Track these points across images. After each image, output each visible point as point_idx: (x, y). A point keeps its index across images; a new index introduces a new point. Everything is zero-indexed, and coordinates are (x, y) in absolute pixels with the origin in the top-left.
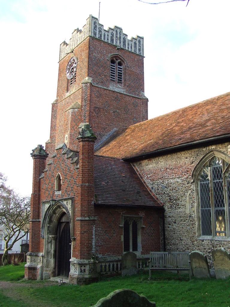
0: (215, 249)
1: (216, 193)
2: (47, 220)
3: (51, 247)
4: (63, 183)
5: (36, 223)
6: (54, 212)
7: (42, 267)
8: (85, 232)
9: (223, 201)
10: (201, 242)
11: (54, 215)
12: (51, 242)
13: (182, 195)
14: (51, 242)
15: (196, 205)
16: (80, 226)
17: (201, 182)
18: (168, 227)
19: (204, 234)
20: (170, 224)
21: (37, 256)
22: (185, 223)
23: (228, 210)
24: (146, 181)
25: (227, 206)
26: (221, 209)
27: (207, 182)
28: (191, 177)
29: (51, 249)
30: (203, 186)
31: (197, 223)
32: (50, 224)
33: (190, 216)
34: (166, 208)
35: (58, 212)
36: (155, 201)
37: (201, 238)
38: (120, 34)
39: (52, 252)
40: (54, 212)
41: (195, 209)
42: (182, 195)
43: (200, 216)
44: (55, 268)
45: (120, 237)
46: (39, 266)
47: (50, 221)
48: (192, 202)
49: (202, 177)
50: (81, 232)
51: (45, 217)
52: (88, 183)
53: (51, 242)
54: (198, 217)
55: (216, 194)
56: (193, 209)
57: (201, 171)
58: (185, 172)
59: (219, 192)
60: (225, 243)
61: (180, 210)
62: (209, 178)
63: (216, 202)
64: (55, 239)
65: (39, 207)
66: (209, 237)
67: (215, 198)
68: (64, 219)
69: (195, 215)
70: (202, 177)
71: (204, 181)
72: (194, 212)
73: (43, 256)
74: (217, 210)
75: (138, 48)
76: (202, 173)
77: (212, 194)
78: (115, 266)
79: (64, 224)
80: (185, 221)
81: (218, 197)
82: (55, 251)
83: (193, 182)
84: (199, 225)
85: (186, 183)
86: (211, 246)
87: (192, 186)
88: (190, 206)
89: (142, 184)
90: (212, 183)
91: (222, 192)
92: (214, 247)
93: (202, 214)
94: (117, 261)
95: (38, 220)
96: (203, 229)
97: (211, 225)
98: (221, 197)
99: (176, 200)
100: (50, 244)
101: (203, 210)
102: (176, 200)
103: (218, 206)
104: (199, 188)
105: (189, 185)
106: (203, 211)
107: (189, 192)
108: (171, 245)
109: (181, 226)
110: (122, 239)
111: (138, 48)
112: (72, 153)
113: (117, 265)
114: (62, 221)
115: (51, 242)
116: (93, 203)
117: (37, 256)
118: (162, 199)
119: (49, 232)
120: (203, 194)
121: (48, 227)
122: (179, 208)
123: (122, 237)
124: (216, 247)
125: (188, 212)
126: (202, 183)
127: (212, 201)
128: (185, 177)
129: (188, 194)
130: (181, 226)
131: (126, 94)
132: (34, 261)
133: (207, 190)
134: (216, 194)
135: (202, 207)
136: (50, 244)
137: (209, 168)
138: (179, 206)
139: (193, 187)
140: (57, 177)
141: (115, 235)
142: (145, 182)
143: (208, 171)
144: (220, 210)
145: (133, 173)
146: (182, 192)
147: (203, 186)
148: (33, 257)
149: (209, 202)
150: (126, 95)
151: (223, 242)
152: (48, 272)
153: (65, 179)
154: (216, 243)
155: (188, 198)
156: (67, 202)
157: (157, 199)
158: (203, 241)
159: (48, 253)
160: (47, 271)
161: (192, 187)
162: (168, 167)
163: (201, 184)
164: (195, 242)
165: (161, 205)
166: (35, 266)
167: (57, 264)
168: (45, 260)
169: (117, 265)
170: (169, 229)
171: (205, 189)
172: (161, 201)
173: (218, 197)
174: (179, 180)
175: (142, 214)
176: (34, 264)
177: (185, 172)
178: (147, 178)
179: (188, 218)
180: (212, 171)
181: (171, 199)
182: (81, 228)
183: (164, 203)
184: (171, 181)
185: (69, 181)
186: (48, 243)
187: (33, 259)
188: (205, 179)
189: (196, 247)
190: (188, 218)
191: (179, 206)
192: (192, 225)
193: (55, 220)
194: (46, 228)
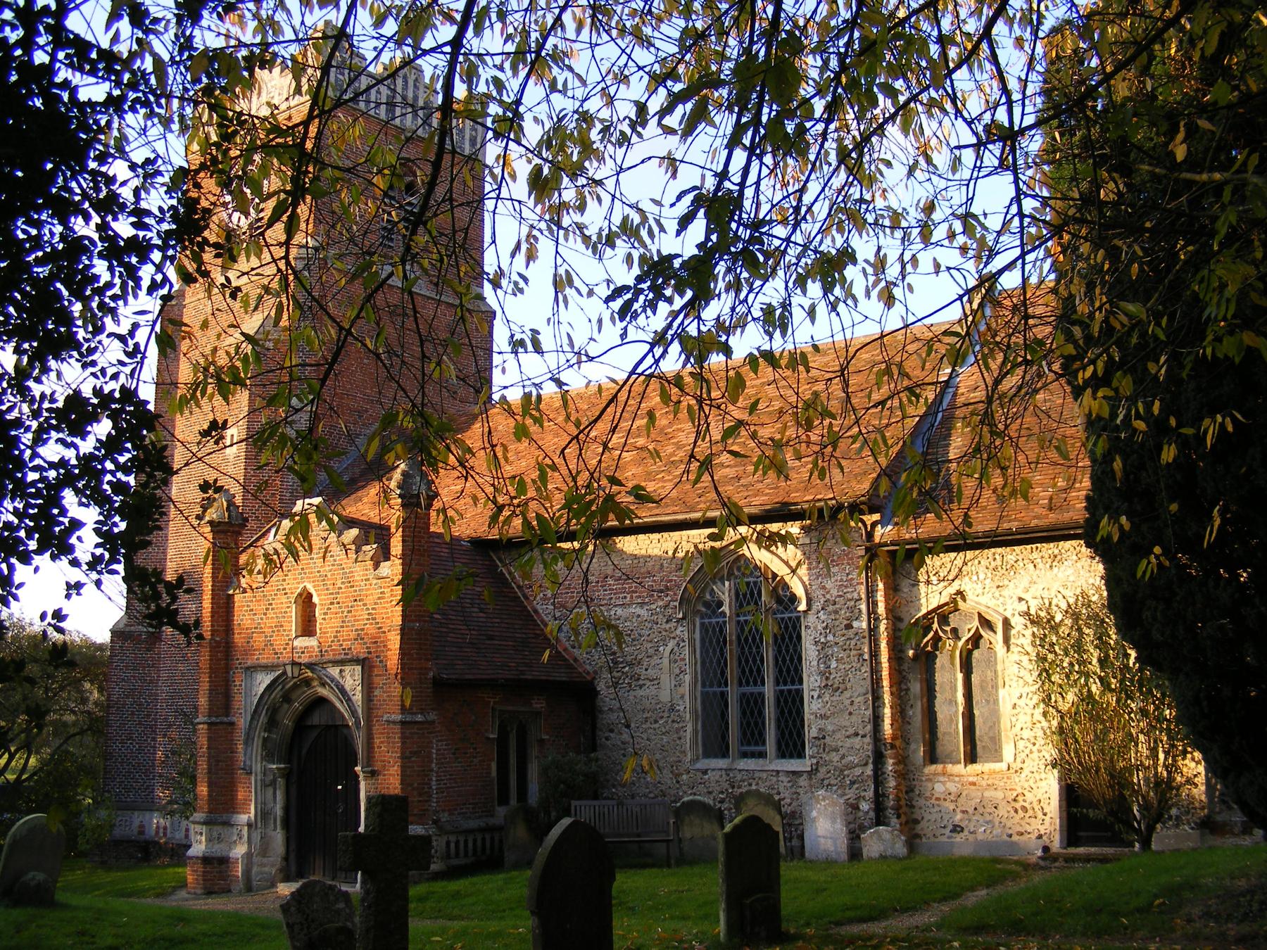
0: (737, 791)
1: (743, 648)
2: (263, 718)
3: (275, 797)
4: (325, 614)
5: (221, 727)
6: (287, 698)
7: (248, 855)
8: (413, 753)
9: (759, 671)
10: (699, 774)
11: (286, 706)
12: (273, 783)
13: (651, 651)
14: (273, 783)
15: (687, 678)
16: (402, 738)
17: (702, 618)
18: (607, 739)
19: (707, 754)
20: (612, 731)
21: (228, 824)
22: (657, 726)
23: (772, 693)
24: (538, 607)
25: (771, 684)
26: (756, 690)
27: (721, 620)
28: (677, 604)
29: (275, 802)
30: (707, 631)
31: (689, 728)
32: (270, 732)
33: (672, 709)
34: (601, 686)
35: (305, 695)
36: (570, 666)
37: (699, 765)
38: (415, 86)
39: (279, 810)
40: (287, 698)
41: (686, 689)
42: (651, 651)
43: (699, 709)
44: (286, 859)
45: (489, 766)
46: (239, 851)
47: (272, 723)
48: (677, 671)
49: (707, 605)
50: (402, 753)
51: (255, 711)
52: (419, 621)
53: (273, 783)
54: (694, 712)
55: (743, 653)
56: (681, 690)
57: (703, 591)
58: (661, 591)
59: (750, 648)
60: (764, 775)
61: (641, 693)
62: (726, 608)
63: (743, 672)
64: (287, 775)
65: (228, 681)
66: (722, 763)
67: (740, 663)
68: (317, 719)
69: (685, 706)
70: (707, 605)
71: (710, 617)
72: (682, 697)
73: (249, 825)
74: (744, 694)
75: (467, 137)
76: (708, 597)
77: (731, 651)
78: (479, 843)
79: (314, 734)
80: (656, 722)
81: (747, 661)
82: (287, 809)
83: (683, 618)
84: (695, 731)
85: (663, 620)
86: (726, 785)
87: (681, 629)
88: (673, 683)
89: (529, 619)
90: (734, 623)
91: (758, 647)
92: (733, 787)
93: (703, 702)
94: (481, 830)
95: (225, 719)
96: (704, 745)
97: (727, 729)
98: (754, 661)
99: (631, 664)
100: (270, 790)
101: (707, 693)
102: (631, 664)
103: (748, 684)
104: (697, 636)
105: (672, 625)
106: (705, 696)
107: (671, 644)
108: (614, 786)
109: (645, 736)
110: (494, 773)
111: (467, 137)
112: (354, 532)
113: (484, 839)
114: (309, 723)
115: (273, 783)
116: (431, 674)
117: (228, 824)
118: (589, 659)
119: (269, 756)
120: (707, 651)
121: (265, 740)
122: (641, 687)
123: (494, 766)
124: (740, 787)
125: (665, 696)
126: (706, 621)
127: (732, 671)
128: (661, 603)
129: (668, 649)
130: (645, 736)
131: (428, 294)
132: (219, 839)
133: (718, 642)
134: (743, 653)
135: (704, 685)
136: (270, 790)
137: (727, 583)
138: (641, 682)
139: (682, 631)
140: (300, 594)
141: (476, 761)
142: (536, 611)
143: (724, 592)
144: (752, 694)
145: (501, 583)
146: (650, 645)
147: (707, 631)
148: (215, 828)
149: (723, 673)
150: (429, 298)
151: (757, 775)
152: (266, 869)
153: (332, 603)
154: (739, 777)
155: (666, 661)
156: (341, 671)
157: (576, 660)
158: (705, 772)
159: (264, 814)
160: (262, 865)
161: (678, 632)
162: (609, 572)
163: (702, 624)
164: (684, 777)
165: (589, 678)
166: (224, 854)
167: (293, 847)
168: (256, 836)
169: (484, 839)
170: (608, 743)
171: (712, 641)
172: (588, 667)
173: (747, 661)
174: (642, 612)
175: (539, 704)
176: (218, 850)
177: (661, 591)
178: (545, 598)
179: (666, 715)
180: (733, 591)
181: (616, 663)
182: (403, 743)
183: (595, 672)
184: (619, 611)
185: (349, 612)
186: (266, 786)
187: (215, 834)
188: (714, 612)
189: (684, 788)
190: (666, 715)
191: (641, 682)
192: (678, 731)
193: (287, 722)
194: (257, 742)
